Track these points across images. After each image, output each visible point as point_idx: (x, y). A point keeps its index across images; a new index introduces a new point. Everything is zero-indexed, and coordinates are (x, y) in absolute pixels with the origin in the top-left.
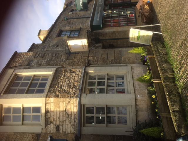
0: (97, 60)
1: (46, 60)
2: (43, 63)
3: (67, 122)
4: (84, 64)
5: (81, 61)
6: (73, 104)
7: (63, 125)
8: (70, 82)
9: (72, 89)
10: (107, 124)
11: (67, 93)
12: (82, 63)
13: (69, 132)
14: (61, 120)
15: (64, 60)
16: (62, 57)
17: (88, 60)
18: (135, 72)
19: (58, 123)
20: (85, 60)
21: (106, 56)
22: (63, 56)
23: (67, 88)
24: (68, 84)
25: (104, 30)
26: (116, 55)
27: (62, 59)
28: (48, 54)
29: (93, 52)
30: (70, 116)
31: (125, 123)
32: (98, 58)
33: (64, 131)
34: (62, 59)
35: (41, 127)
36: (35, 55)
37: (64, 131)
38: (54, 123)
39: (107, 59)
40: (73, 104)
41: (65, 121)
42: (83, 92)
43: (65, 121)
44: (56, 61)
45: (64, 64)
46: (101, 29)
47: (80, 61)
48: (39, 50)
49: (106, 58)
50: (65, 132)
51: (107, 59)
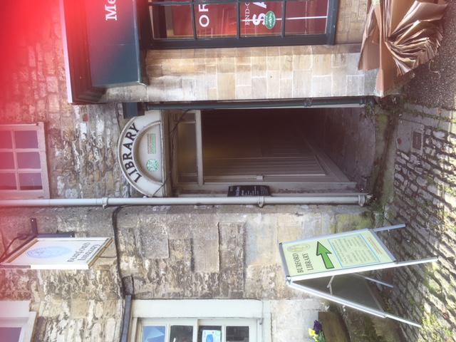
0: (153, 275)
4: (108, 291)
17: (119, 271)
20: (106, 269)
21: (188, 256)
25: (162, 85)
39: (193, 268)
45: (33, 289)
49: (188, 263)
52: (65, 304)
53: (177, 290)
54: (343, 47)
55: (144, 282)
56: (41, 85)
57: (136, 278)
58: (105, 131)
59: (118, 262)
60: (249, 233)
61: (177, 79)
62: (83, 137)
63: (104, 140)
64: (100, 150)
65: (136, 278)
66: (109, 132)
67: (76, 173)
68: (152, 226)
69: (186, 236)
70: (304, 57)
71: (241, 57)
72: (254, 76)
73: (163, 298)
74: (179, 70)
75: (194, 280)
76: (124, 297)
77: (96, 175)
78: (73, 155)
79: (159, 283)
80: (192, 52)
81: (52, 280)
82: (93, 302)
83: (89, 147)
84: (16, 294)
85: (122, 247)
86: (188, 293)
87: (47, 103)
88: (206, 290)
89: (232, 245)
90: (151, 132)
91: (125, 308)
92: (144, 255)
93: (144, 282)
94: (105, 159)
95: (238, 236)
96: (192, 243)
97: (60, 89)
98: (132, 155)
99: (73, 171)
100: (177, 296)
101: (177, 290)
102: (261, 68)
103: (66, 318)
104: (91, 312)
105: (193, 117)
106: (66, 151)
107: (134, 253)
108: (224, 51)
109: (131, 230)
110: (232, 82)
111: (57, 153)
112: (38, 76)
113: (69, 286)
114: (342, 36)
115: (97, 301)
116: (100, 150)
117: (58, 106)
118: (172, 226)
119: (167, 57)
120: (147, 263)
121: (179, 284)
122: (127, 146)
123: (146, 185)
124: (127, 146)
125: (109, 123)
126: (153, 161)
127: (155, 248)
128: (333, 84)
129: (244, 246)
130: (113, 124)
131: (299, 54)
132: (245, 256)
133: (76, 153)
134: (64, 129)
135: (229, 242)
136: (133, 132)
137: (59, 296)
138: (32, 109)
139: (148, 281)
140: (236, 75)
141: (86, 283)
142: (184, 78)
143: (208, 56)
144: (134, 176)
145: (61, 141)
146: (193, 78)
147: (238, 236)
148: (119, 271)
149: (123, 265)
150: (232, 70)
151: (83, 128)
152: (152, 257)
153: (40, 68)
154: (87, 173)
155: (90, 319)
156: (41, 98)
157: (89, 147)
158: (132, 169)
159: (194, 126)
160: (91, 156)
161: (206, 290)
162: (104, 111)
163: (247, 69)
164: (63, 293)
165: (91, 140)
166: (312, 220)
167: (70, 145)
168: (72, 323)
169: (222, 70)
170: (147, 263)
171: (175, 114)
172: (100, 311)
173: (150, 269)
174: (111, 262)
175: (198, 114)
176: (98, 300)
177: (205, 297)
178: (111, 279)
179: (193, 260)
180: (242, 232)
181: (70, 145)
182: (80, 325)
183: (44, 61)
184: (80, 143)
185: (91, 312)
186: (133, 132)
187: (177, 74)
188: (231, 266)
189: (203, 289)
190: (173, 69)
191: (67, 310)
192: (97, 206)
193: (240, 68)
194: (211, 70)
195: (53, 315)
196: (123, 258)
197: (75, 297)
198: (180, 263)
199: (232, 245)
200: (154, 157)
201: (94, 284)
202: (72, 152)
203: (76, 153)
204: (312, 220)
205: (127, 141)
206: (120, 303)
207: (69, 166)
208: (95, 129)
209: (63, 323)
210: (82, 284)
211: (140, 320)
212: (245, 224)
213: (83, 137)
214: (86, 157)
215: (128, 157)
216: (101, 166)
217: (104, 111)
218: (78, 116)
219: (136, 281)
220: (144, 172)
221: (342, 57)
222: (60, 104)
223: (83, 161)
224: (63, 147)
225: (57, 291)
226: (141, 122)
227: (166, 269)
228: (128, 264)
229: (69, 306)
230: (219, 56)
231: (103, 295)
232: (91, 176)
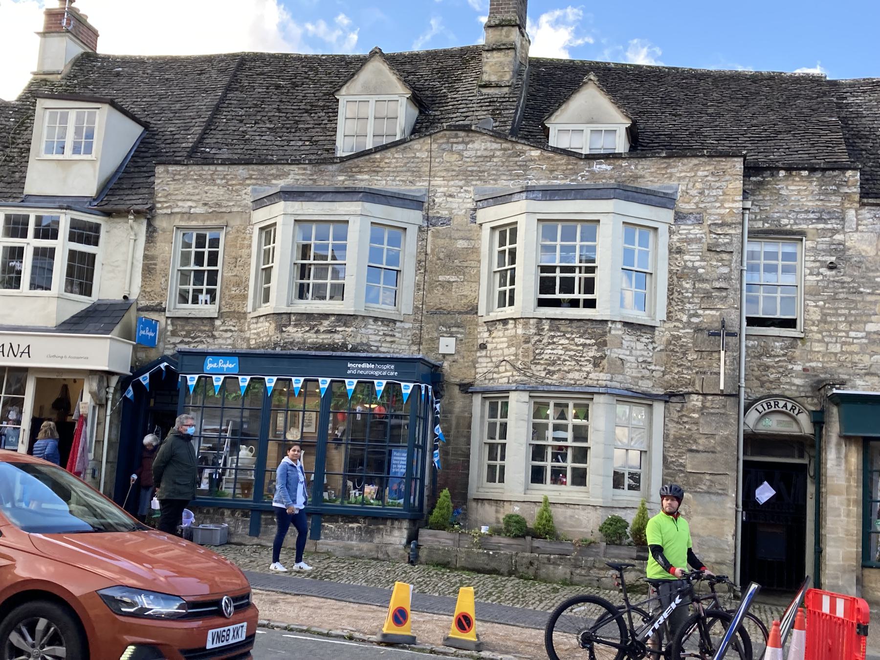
0: (685, 419)
1: (697, 264)
2: (686, 257)
3: (490, 365)
4: (672, 382)
5: (685, 372)
6: (513, 376)
7: (486, 356)
8: (565, 360)
9: (545, 369)
10: (489, 444)
11: (535, 359)
12: (677, 377)
13: (478, 370)
14: (494, 353)
15: (695, 320)
16: (707, 312)
17: (689, 393)
18: (582, 513)
19: (489, 346)
20: (692, 383)
21: (701, 448)
22: (713, 312)
23: (547, 357)
24: (559, 359)
25: (838, 445)
26: (708, 477)
27: (700, 312)
28: (727, 263)
29: (724, 407)
30: (496, 370)
31: (491, 479)
32: (696, 423)
33: (480, 360)
34: (700, 312)
35: (484, 314)
36: (722, 225)
37: (480, 360)
38: (490, 340)
39: (691, 451)
40: (513, 376)
41: (492, 361)
42: (532, 394)
43: (492, 361)
44: (693, 297)
45: (677, 324)
46: (450, 427)
47: (688, 368)
48: (810, 204)
49: (694, 448)
50: (478, 363)
51: (691, 451)
52: (662, 347)
53: (671, 437)
54: (860, 572)
55: (679, 411)
56: (834, 339)
57: (683, 406)
58: (794, 385)
59: (698, 394)
60: (720, 498)
61: (843, 456)
62: (790, 367)
63: (787, 383)
64: (779, 379)
65: (683, 406)
66: (794, 388)
67: (759, 357)
68: (727, 424)
69: (719, 449)
70: (855, 544)
71: (856, 502)
72: (843, 510)
73: (665, 425)
74: (849, 458)
75: (679, 450)
76: (665, 394)
77: (757, 373)
78: (775, 356)
79: (678, 423)
80: (861, 467)
81: (683, 340)
82: (663, 369)
83: (781, 370)
84: (672, 309)
85: (710, 398)
86: (667, 445)
87: (819, 341)
88: (670, 460)
89: (708, 483)
90: (794, 424)
91: (657, 395)
92: (703, 414)
93: (679, 411)
94: (771, 382)
95: (717, 488)
96: (713, 452)
97: (830, 353)
98: (777, 409)
99: (761, 355)
100: (666, 437)
101: (671, 437)
102: (848, 515)
103: (654, 348)
104: (657, 368)
105: (801, 456)
106: (779, 352)
107: (704, 407)
108: (861, 490)
109: (724, 407)
110: (839, 493)
111: (777, 344)
112: (842, 337)
113: (677, 352)
114: (867, 572)
115: (663, 372)
116: (779, 379)
117: (817, 350)
118: (727, 438)
119: (858, 450)
120: (696, 415)
121: (676, 439)
122: (785, 406)
123: (753, 415)
124: (785, 406)
125: (802, 389)
126: (770, 423)
127: (709, 424)
128: (835, 563)
129: (709, 493)
130: (800, 392)
131: (857, 541)
132: (699, 492)
133: (777, 359)
134: (797, 353)
135: (711, 481)
136: (796, 411)
137: (669, 343)
138: (815, 328)
139: (680, 414)
140: (844, 497)
141: (679, 366)
142: (843, 461)
143: (858, 479)
144: (760, 408)
145: (787, 348)
146: (843, 467)
147: (717, 488)
148: (689, 393)
149: (694, 397)
150: (847, 494)
151: (798, 368)
152: (701, 421)
153: (848, 340)
154: (759, 366)
155: (653, 367)
156: (823, 337)
157: (781, 370)
158: (766, 407)
159: (793, 457)
160: (774, 371)
161: (670, 460)
162: (811, 386)
163: (849, 505)
164: (672, 347)
165: (787, 373)
166: (728, 545)
167: (784, 355)
168: (651, 354)
169: (848, 487)
170: (696, 415)
171: (811, 446)
172: (657, 375)
173: (691, 417)
174: (698, 388)
175: (206, 274)
176: (664, 373)
177: (665, 458)
178: (681, 386)
179: (697, 451)
180: (720, 492)
181: (784, 355)
182: (649, 360)
183: (853, 343)
184: (785, 364)
185: (657, 368)
186: (796, 411)
187: (846, 456)
188: (691, 480)
189: (672, 457)
190: (850, 454)
191: (658, 349)
192: (739, 378)
193: (849, 500)
194: (848, 480)
195: (656, 339)
196: (700, 397)
197: (667, 355)
198: (695, 441)
199: (708, 483)
200: (774, 425)
201: (678, 372)
202: (778, 356)
203: (777, 359)
204: (728, 545)
205: (789, 406)
206: (661, 391)
207: (767, 353)
208: (796, 377)
209: (650, 347)
210: (679, 362)
211: (651, 405)
212: (727, 495)
213: (790, 367)
214: (773, 367)
215: (776, 405)
216: (765, 378)
217: (811, 386)
218: (808, 365)
219: (680, 405)
220: (763, 416)
221: (853, 571)
222: (819, 352)
223: (771, 364)
224: (782, 349)
225: (673, 342)
226: (804, 419)
227: (689, 430)
228: (696, 401)
229: (661, 350)
230: (857, 487)
231: (667, 377)
232: (756, 369)
